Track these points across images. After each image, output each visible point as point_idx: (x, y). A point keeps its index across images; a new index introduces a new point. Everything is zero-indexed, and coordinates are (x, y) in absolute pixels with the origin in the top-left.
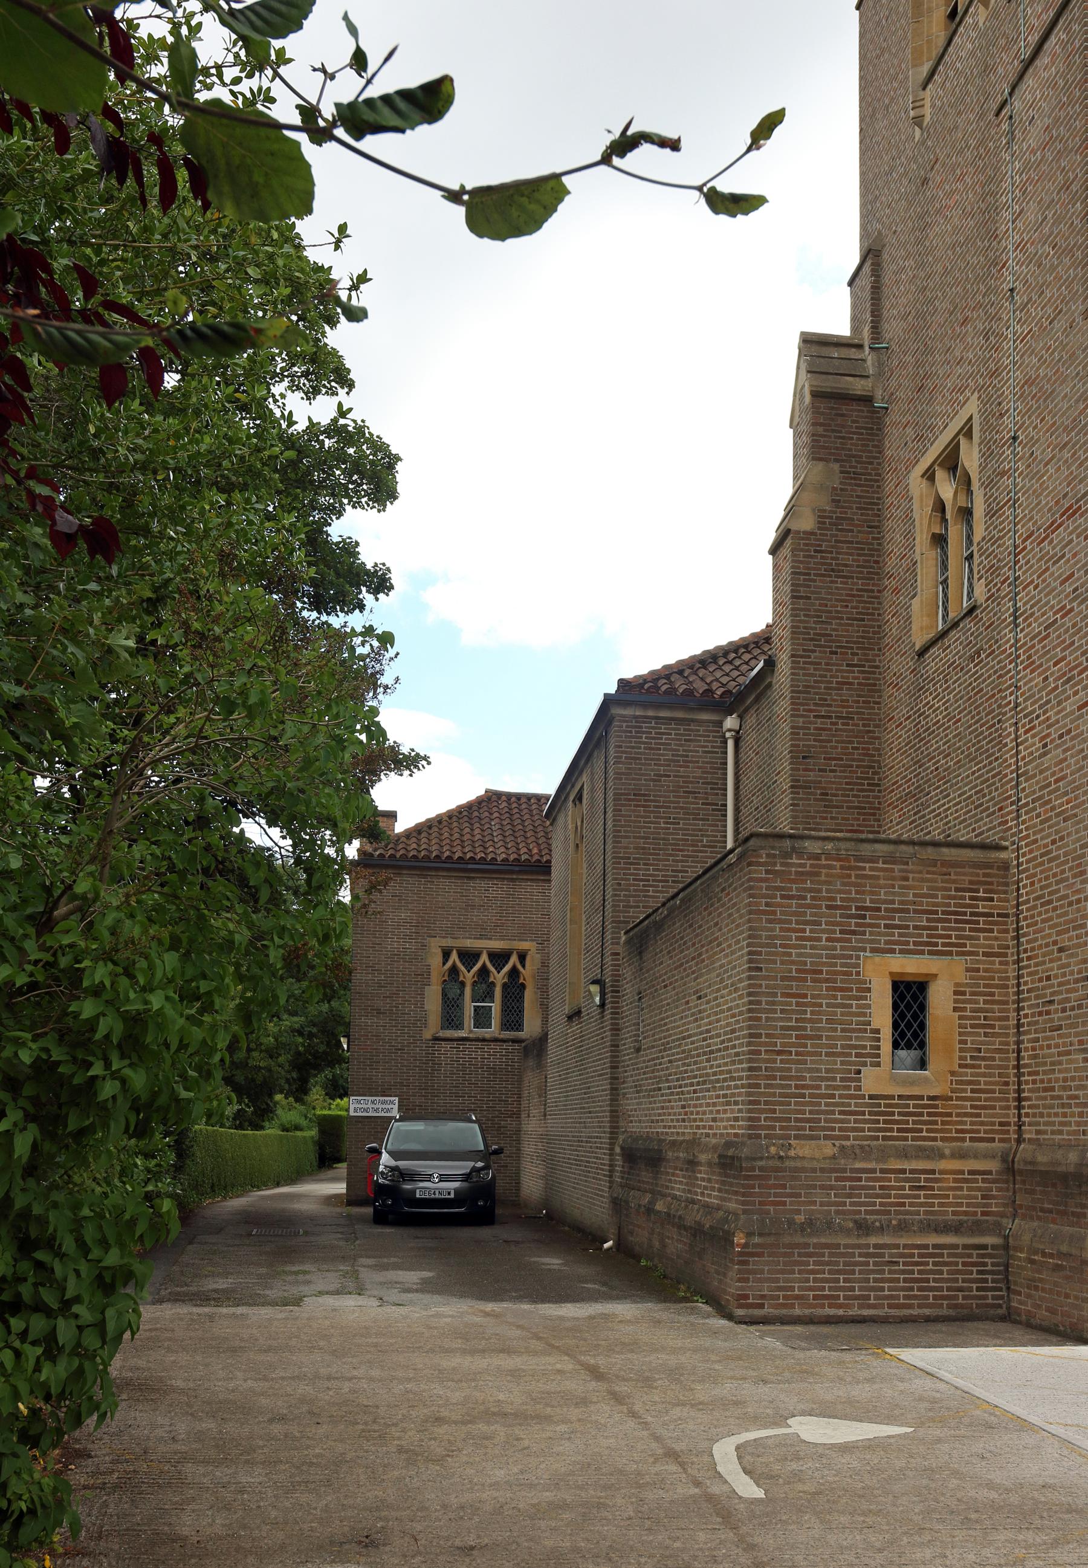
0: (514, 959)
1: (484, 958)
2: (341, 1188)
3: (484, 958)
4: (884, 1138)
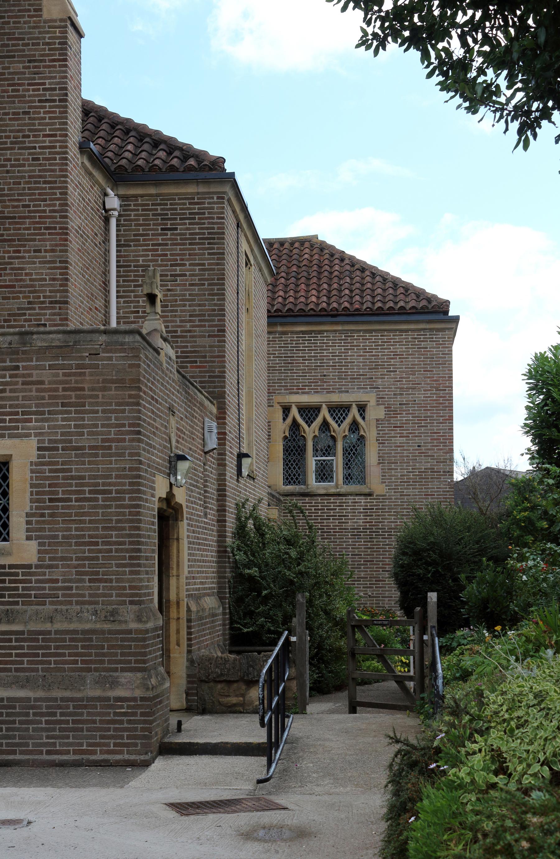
0: (354, 411)
1: (325, 412)
2: (411, 628)
3: (325, 412)
4: (17, 670)
